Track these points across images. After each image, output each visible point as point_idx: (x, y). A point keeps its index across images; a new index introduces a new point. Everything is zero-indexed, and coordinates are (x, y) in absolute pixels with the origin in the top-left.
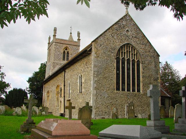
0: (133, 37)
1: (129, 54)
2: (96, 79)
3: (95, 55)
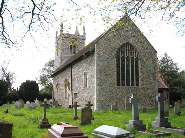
0: (132, 36)
1: (129, 52)
2: (99, 76)
3: (98, 56)
